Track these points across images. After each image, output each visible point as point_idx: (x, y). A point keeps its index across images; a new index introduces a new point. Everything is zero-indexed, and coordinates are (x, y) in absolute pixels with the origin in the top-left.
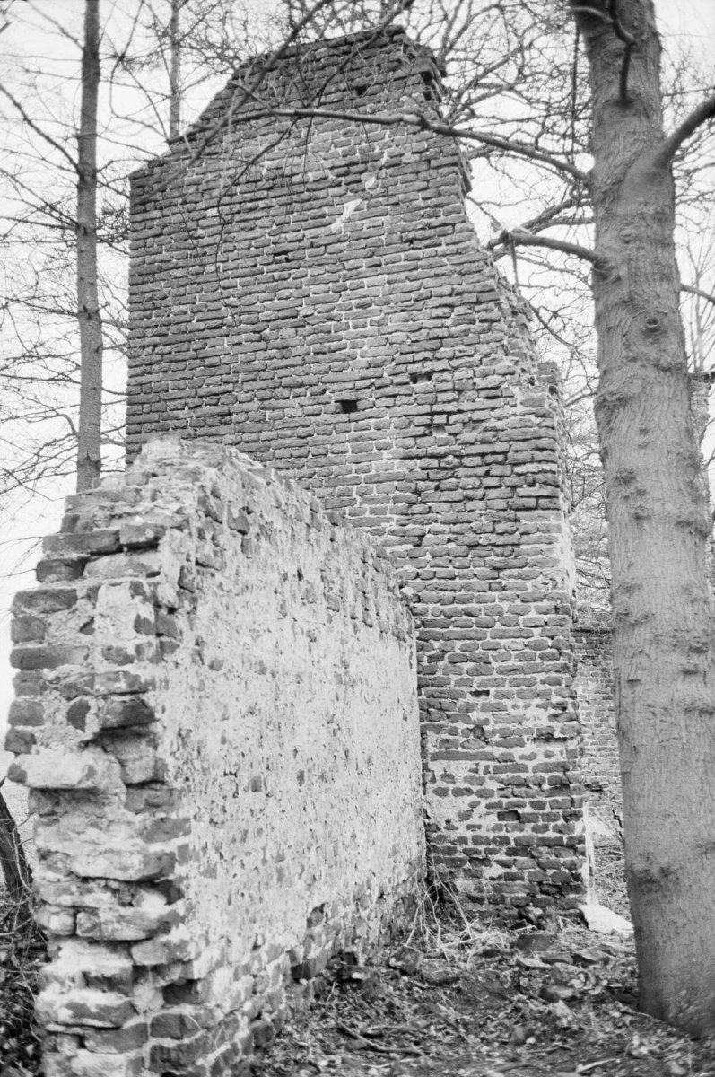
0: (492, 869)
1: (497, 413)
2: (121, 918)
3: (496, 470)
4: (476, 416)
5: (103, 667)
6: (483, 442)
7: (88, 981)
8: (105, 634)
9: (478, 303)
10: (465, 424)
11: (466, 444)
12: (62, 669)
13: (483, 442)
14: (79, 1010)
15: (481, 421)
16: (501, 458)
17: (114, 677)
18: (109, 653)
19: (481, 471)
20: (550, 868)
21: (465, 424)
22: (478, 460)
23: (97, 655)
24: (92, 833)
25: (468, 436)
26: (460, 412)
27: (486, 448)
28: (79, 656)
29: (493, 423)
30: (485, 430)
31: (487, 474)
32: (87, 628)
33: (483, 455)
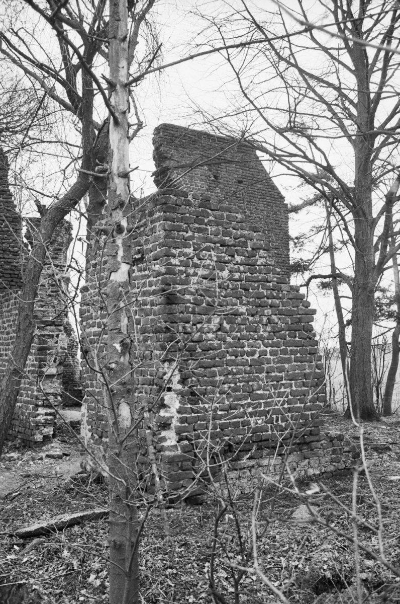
0: (321, 299)
1: (17, 261)
2: (54, 401)
3: (15, 280)
4: (9, 260)
5: (60, 350)
6: (11, 270)
7: (46, 414)
8: (60, 344)
9: (13, 222)
10: (5, 262)
11: (5, 269)
12: (52, 351)
13: (11, 270)
14: (46, 420)
15: (10, 262)
16: (17, 276)
17: (63, 353)
18: (62, 348)
19: (10, 279)
20: (338, 277)
21: (5, 262)
22: (9, 276)
23: (59, 348)
24: (50, 384)
25: (7, 267)
26: (4, 258)
27: (12, 272)
28: (55, 348)
29: (15, 264)
30: (12, 266)
31: (12, 281)
32: (57, 342)
33: (10, 274)
